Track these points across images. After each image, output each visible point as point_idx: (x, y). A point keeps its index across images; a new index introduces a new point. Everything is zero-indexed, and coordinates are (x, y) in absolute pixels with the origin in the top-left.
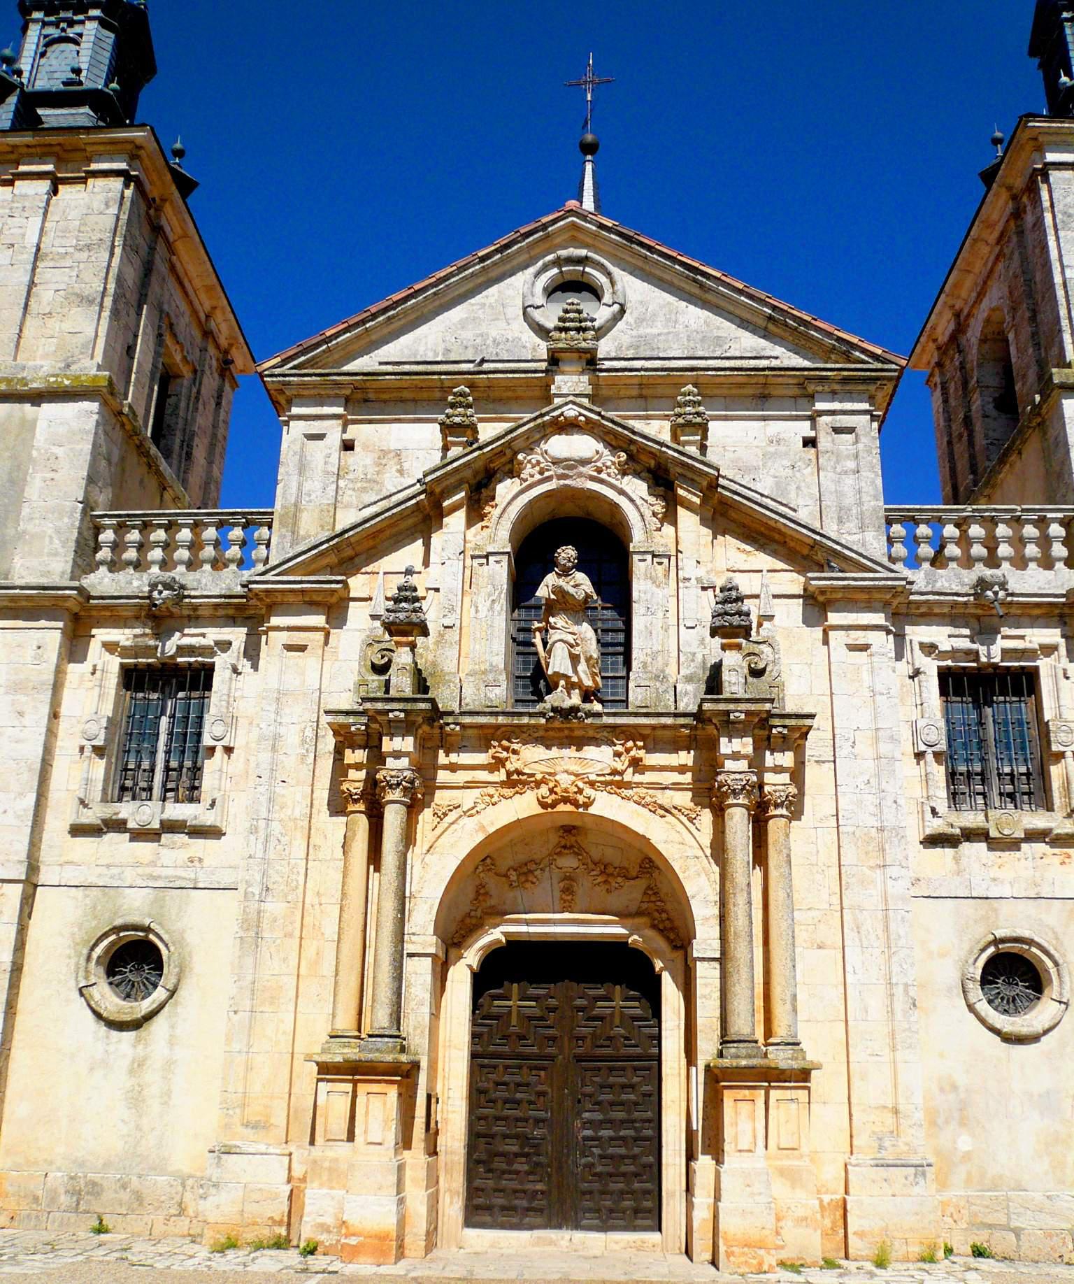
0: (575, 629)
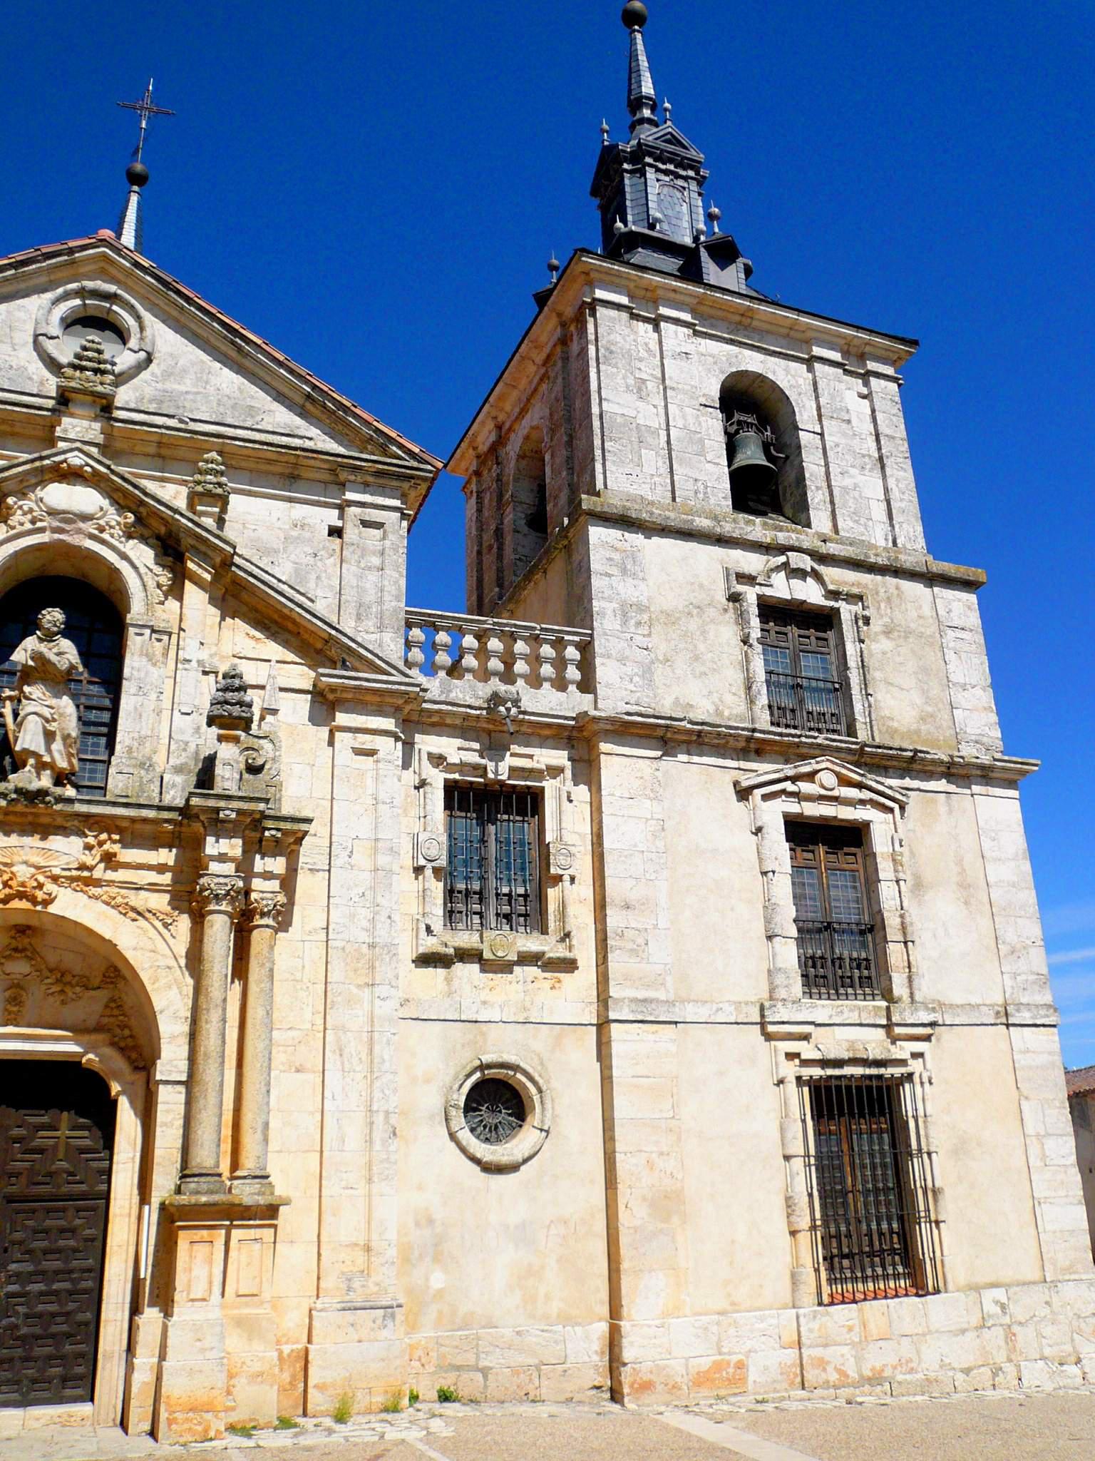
0: (53, 702)
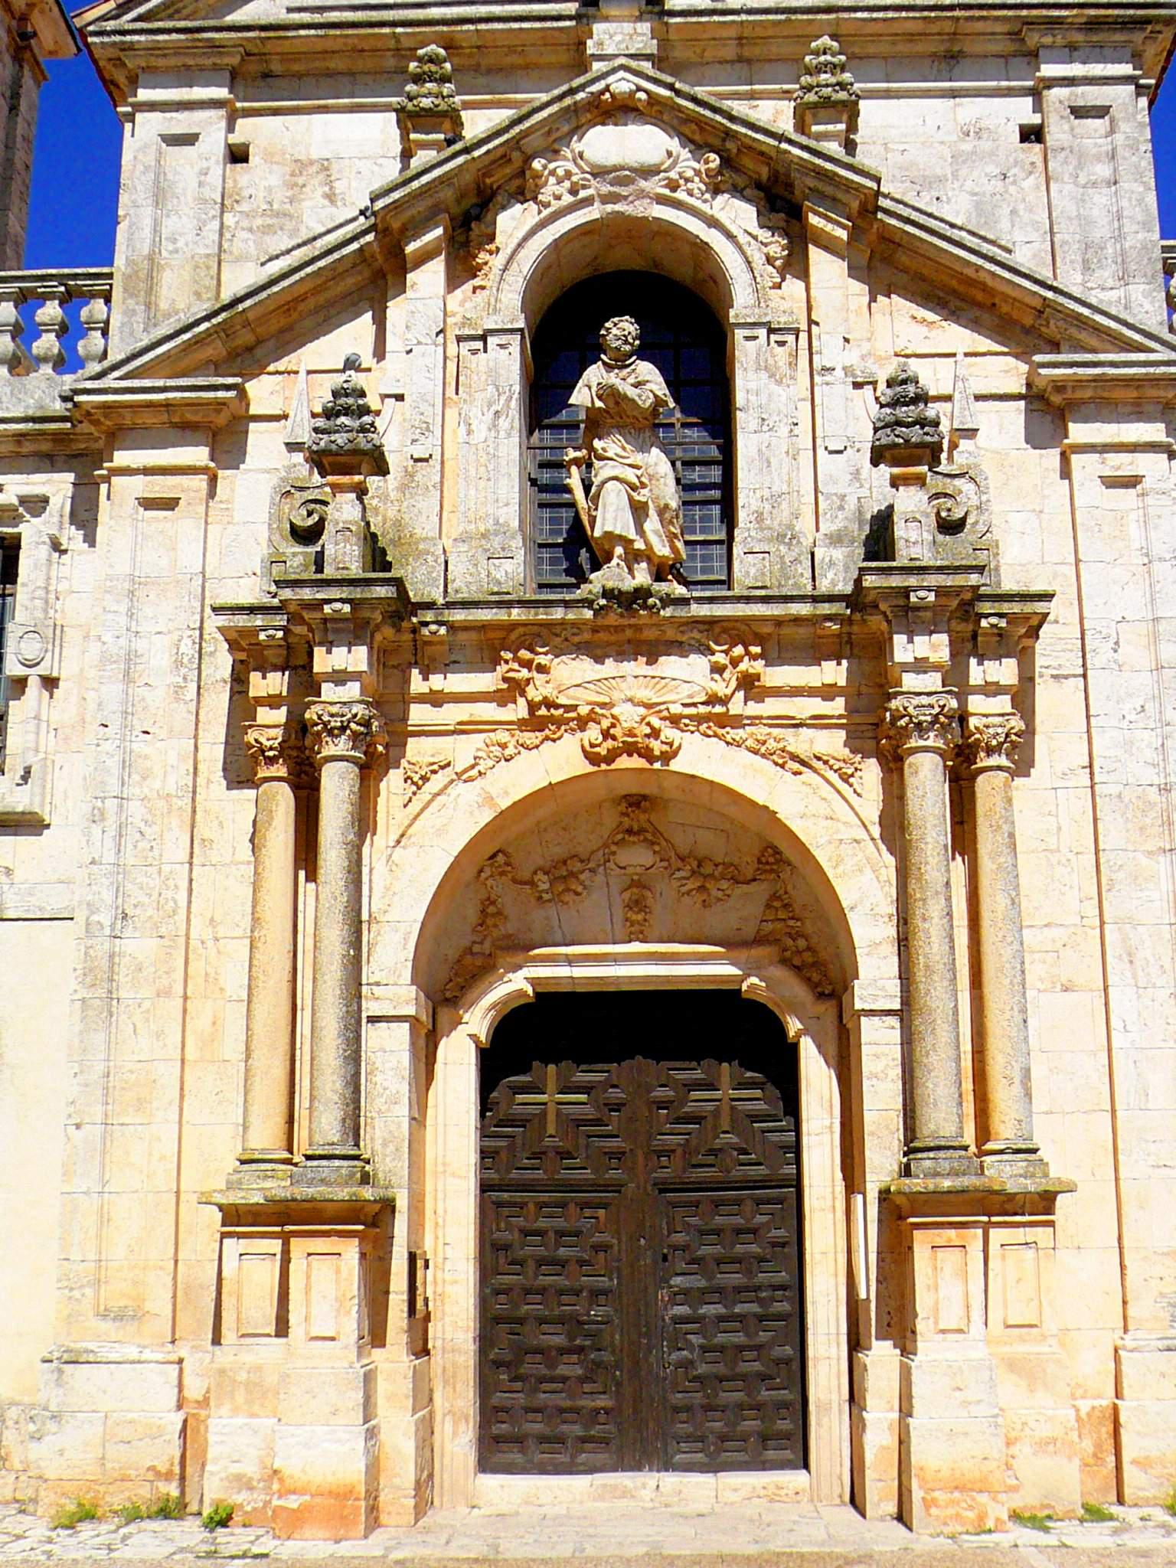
0: (638, 458)
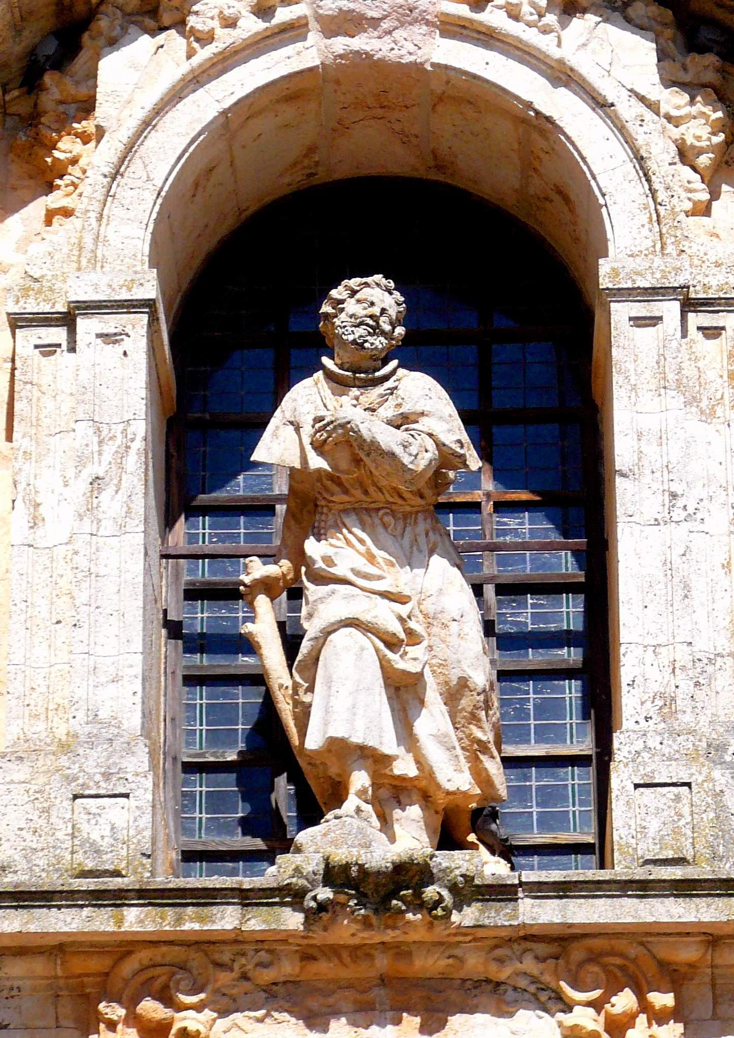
0: (401, 579)
